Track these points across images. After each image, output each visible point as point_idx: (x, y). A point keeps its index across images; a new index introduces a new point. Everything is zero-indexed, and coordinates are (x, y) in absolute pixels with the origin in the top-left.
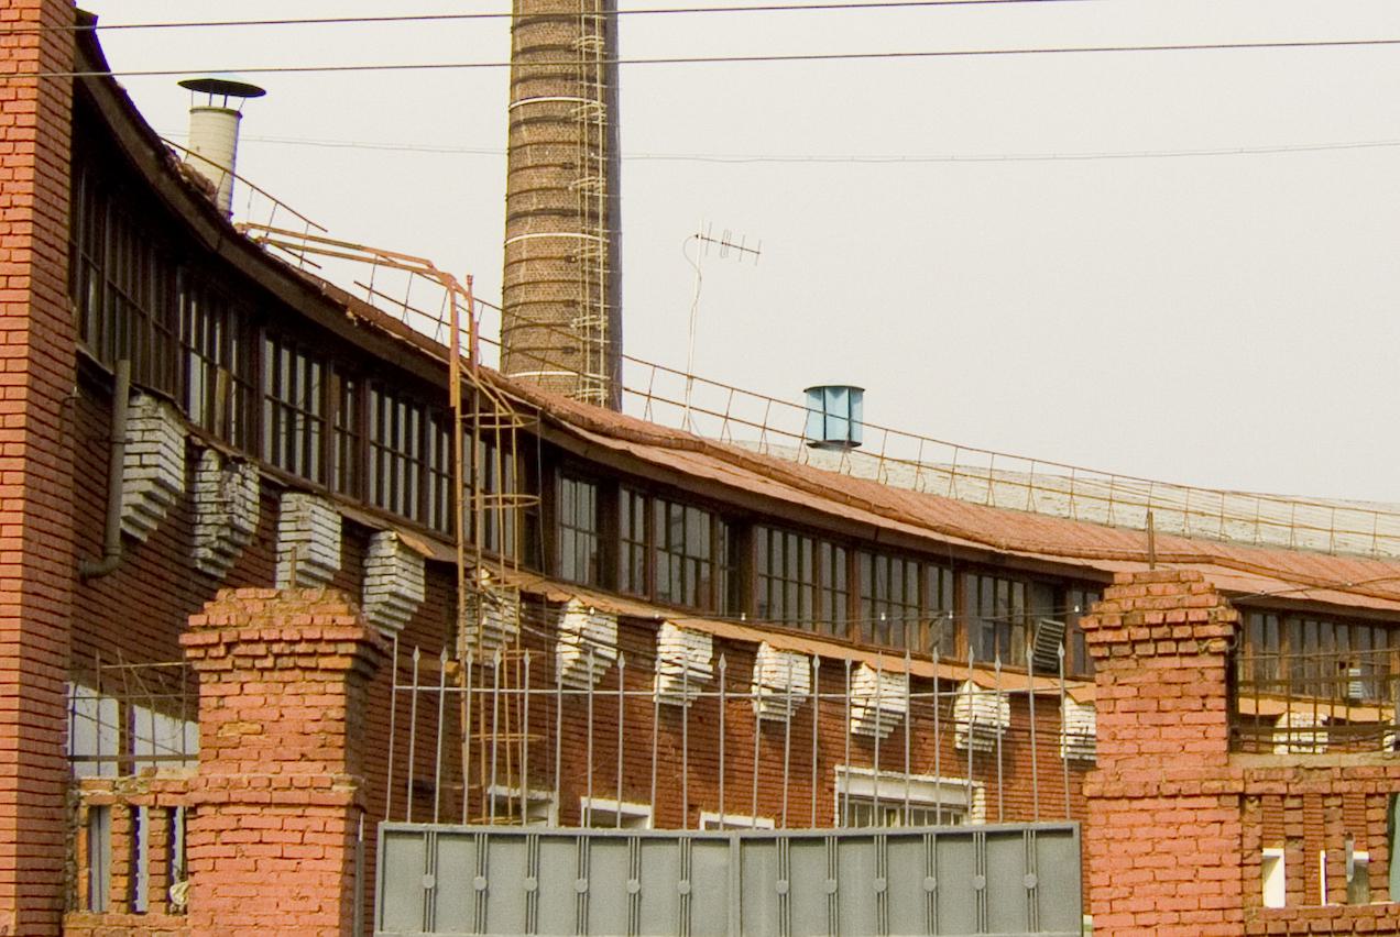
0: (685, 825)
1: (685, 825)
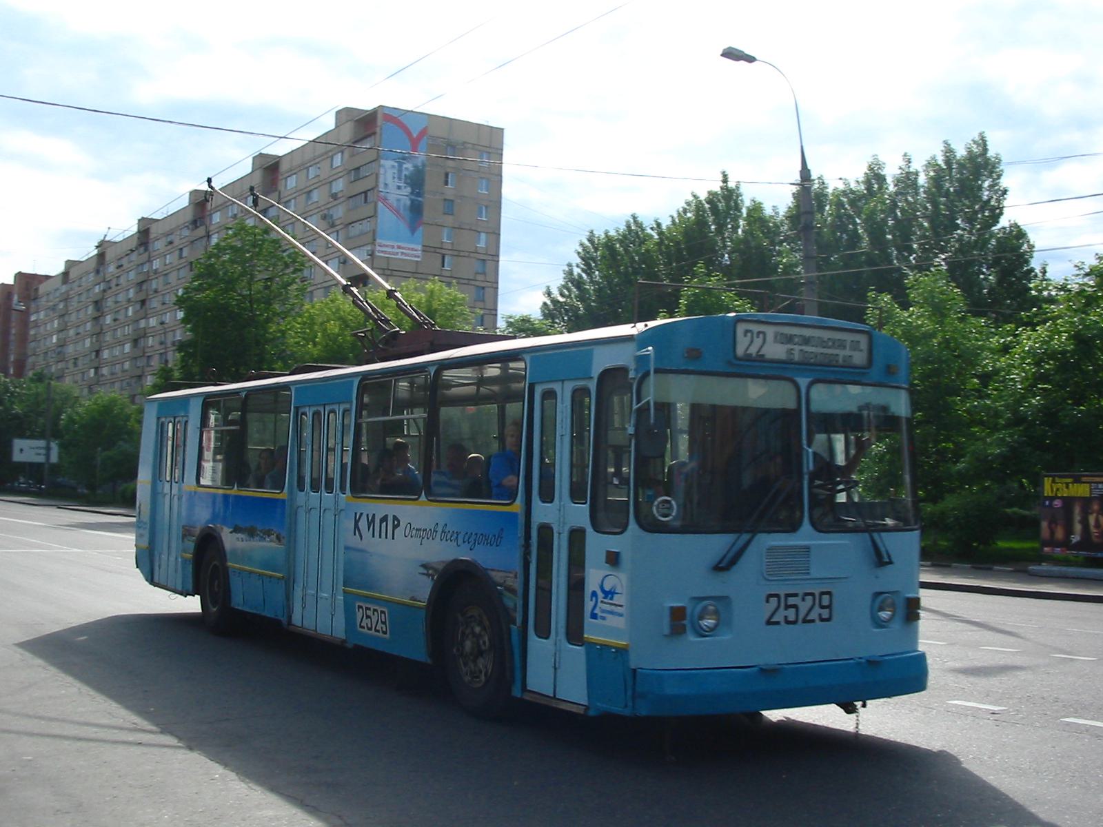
0: (848, 348)
1: (848, 348)
